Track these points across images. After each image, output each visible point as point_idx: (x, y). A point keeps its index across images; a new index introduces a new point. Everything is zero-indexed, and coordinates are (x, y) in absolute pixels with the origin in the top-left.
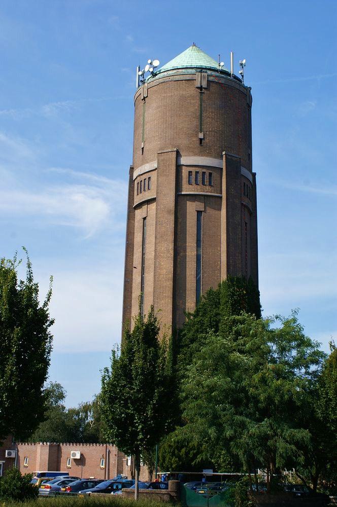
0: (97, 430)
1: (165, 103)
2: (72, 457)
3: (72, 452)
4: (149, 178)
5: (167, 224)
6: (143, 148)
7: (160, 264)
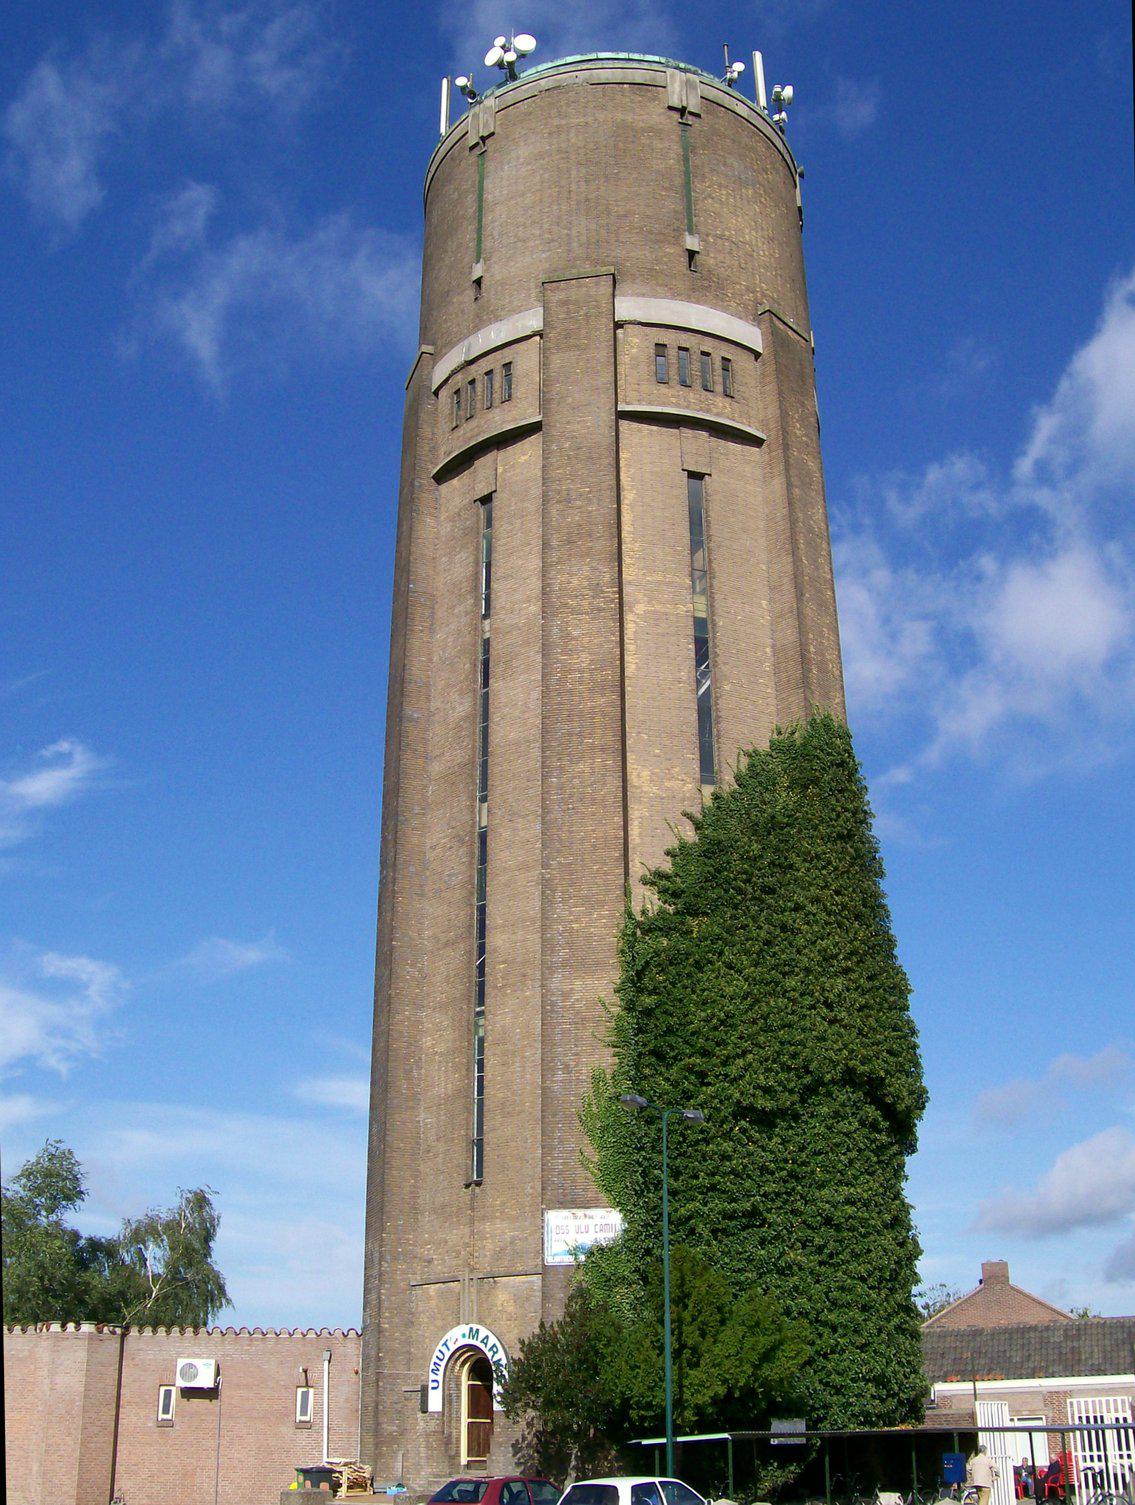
0: (680, 839)
1: (451, 309)
2: (181, 1383)
3: (181, 1362)
4: (507, 366)
5: (589, 500)
6: (478, 282)
7: (567, 637)
